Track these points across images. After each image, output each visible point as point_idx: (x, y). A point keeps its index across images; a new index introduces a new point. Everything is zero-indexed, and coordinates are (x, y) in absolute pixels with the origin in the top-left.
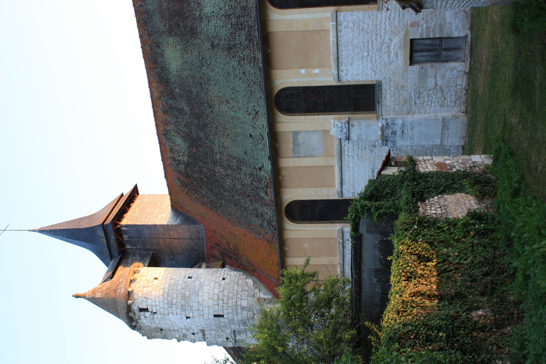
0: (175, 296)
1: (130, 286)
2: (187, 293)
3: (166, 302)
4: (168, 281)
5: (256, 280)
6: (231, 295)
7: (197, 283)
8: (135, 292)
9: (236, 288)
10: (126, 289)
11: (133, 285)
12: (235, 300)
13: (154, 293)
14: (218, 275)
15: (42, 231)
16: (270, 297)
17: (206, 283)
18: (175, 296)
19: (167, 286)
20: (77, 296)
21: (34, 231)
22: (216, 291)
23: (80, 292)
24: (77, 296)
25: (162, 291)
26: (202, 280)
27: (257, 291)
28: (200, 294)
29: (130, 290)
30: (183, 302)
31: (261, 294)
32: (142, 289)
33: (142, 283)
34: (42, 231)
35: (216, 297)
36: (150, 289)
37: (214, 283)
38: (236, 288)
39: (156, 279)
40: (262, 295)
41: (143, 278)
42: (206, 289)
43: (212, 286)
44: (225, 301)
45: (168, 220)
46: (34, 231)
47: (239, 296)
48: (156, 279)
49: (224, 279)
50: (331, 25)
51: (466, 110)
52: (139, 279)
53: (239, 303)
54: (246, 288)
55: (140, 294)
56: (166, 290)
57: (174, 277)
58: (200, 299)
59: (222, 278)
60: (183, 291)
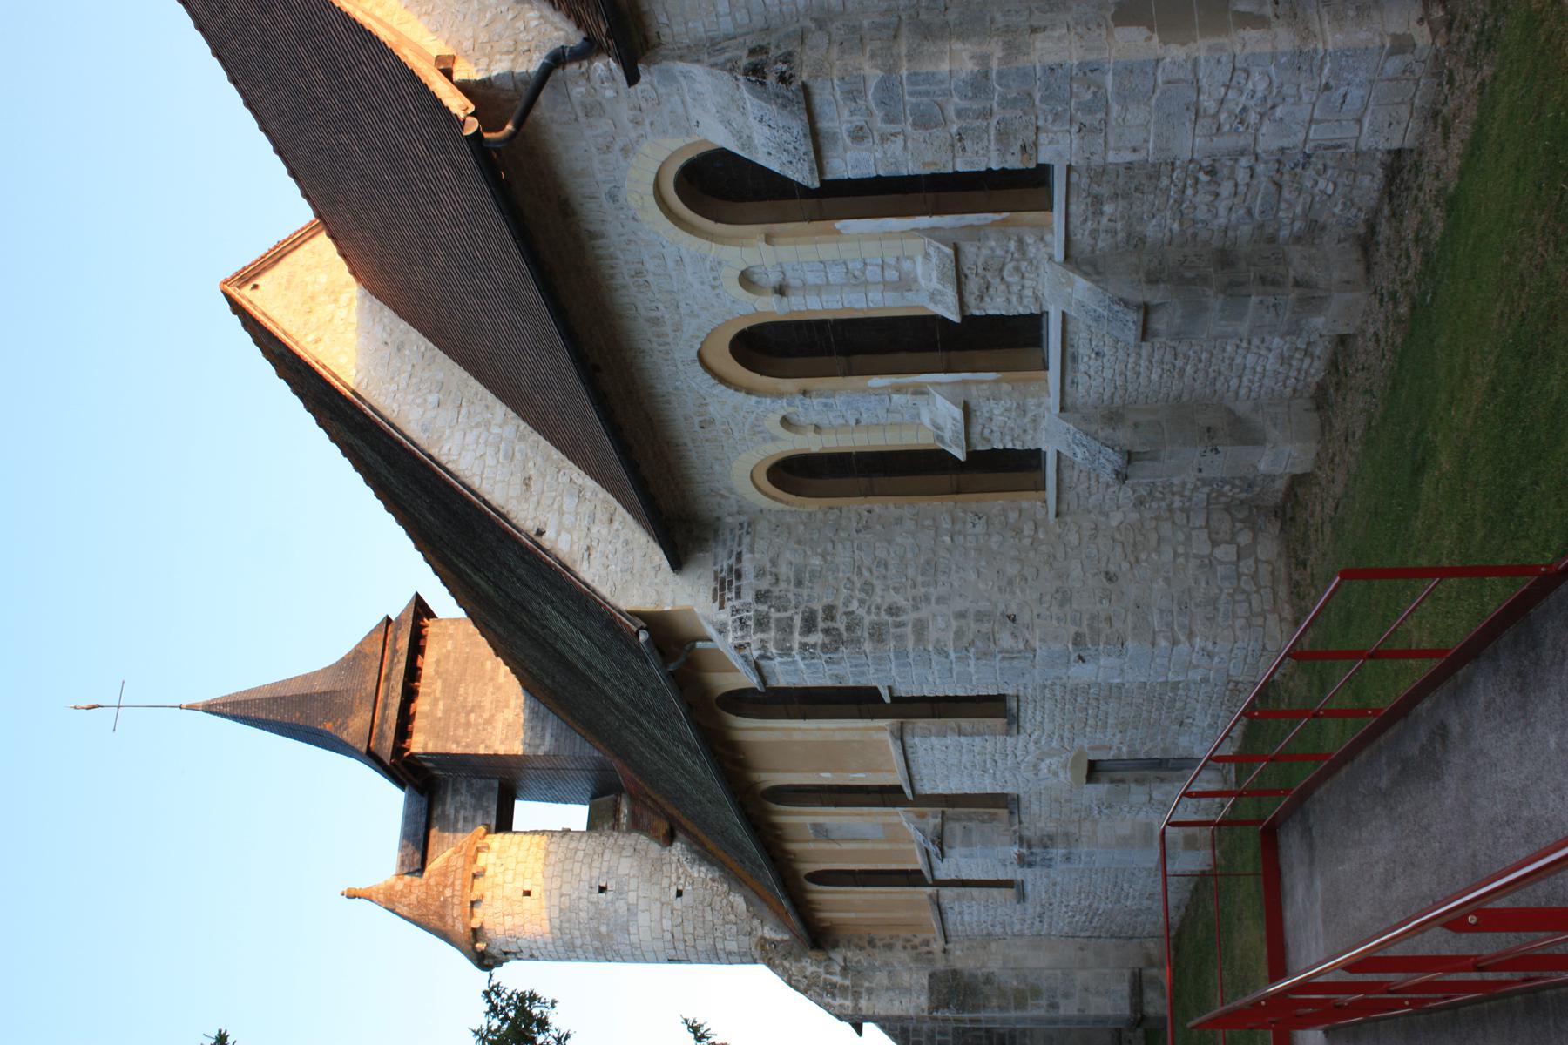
0: (577, 933)
1: (472, 915)
2: (603, 929)
3: (559, 943)
4: (555, 900)
5: (752, 896)
6: (700, 932)
7: (622, 906)
8: (486, 926)
9: (709, 917)
10: (465, 925)
11: (478, 911)
12: (710, 941)
13: (528, 927)
14: (665, 882)
15: (210, 708)
16: (787, 937)
17: (642, 904)
18: (577, 933)
19: (555, 913)
20: (352, 895)
21: (190, 707)
22: (667, 924)
23: (360, 884)
24: (352, 895)
25: (546, 925)
26: (632, 897)
27: (756, 922)
28: (632, 930)
29: (475, 924)
30: (597, 944)
31: (766, 929)
32: (500, 920)
33: (498, 905)
34: (210, 708)
35: (668, 936)
36: (518, 920)
37: (658, 904)
38: (709, 917)
39: (527, 893)
40: (768, 932)
41: (498, 891)
42: (643, 919)
43: (656, 916)
44: (690, 942)
45: (522, 736)
46: (190, 707)
47: (718, 934)
48: (527, 893)
49: (679, 893)
50: (930, 915)
51: (1365, 153)
52: (488, 895)
53: (720, 946)
54: (732, 917)
55: (499, 930)
56: (556, 923)
57: (566, 889)
58: (634, 939)
59: (674, 893)
60: (594, 924)
